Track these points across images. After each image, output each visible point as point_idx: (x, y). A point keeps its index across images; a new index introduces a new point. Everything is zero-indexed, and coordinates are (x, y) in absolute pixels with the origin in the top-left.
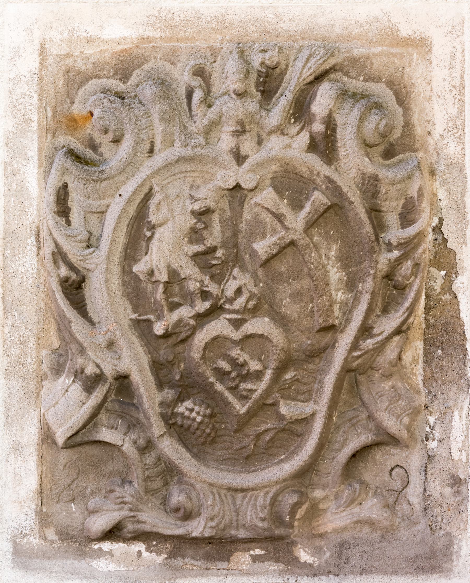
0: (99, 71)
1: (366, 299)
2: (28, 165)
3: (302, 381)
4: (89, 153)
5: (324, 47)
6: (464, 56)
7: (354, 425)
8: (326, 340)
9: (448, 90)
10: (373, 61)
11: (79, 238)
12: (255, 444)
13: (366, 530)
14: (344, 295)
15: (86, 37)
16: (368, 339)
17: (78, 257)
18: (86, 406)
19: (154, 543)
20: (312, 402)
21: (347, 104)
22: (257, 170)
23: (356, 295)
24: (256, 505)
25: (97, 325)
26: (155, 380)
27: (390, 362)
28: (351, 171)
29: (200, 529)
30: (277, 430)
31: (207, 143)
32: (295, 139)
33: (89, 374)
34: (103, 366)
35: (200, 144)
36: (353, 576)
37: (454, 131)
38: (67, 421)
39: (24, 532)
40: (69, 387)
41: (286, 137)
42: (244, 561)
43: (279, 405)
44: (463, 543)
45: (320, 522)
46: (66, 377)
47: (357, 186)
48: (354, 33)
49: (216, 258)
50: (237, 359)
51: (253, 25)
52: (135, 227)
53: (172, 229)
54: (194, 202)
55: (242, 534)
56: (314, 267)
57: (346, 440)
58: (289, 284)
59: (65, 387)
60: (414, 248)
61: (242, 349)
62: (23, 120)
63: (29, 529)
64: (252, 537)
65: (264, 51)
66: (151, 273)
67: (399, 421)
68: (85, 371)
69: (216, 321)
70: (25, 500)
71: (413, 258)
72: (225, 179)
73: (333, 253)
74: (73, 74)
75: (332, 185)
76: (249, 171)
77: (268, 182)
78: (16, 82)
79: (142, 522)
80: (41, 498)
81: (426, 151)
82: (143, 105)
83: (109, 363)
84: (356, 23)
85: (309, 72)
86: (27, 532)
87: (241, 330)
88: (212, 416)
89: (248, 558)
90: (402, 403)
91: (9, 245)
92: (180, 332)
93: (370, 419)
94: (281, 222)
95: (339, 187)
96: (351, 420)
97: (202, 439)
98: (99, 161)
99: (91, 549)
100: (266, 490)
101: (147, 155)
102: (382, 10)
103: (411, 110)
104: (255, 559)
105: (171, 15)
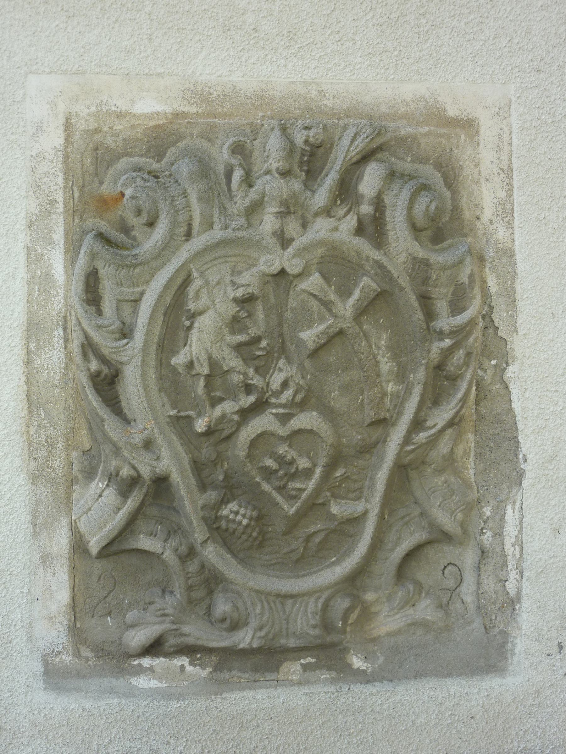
0: (130, 148)
1: (418, 390)
2: (54, 250)
3: (353, 478)
4: (120, 237)
5: (370, 125)
6: (511, 139)
7: (406, 523)
8: (376, 435)
9: (496, 174)
10: (420, 141)
11: (111, 328)
12: (305, 547)
13: (420, 632)
14: (394, 387)
15: (115, 112)
16: (421, 432)
17: (110, 350)
18: (122, 511)
19: (199, 656)
20: (363, 500)
21: (396, 186)
22: (303, 254)
23: (407, 386)
24: (306, 611)
25: (133, 423)
26: (197, 481)
27: (444, 456)
28: (400, 256)
29: (248, 639)
30: (327, 532)
31: (250, 225)
32: (342, 221)
33: (124, 477)
34: (140, 467)
35: (242, 226)
36: (407, 680)
37: (503, 216)
38: (101, 528)
39: (56, 650)
40: (103, 491)
41: (332, 219)
42: (294, 671)
43: (330, 504)
44: (518, 641)
45: (373, 625)
46: (99, 481)
47: (407, 272)
48: (400, 112)
49: (261, 348)
50: (284, 457)
51: (295, 101)
52: (172, 316)
53: (213, 317)
54: (237, 288)
55: (292, 643)
56: (364, 357)
57: (399, 538)
58: (338, 376)
59: (99, 491)
60: (466, 336)
61: (290, 446)
62: (47, 201)
63: (61, 646)
64: (302, 645)
65: (307, 128)
66: (190, 365)
67: (453, 518)
68: (121, 473)
69: (262, 416)
70: (57, 615)
71: (466, 347)
72: (269, 264)
73: (383, 343)
74: (102, 151)
75: (381, 270)
76: (295, 255)
77: (314, 268)
78: (39, 160)
79: (185, 635)
80: (73, 612)
81: (475, 236)
82: (180, 185)
83: (146, 464)
84: (402, 102)
85: (356, 151)
86: (60, 650)
87: (288, 426)
88: (259, 518)
89: (299, 667)
90: (456, 498)
91: (34, 337)
92: (223, 429)
93: (422, 516)
94: (329, 310)
95: (389, 272)
96: (403, 518)
97: (248, 544)
98: (132, 245)
99: (130, 665)
100: (317, 595)
101: (184, 238)
102: (428, 89)
103: (459, 193)
104: (305, 668)
105: (207, 89)
